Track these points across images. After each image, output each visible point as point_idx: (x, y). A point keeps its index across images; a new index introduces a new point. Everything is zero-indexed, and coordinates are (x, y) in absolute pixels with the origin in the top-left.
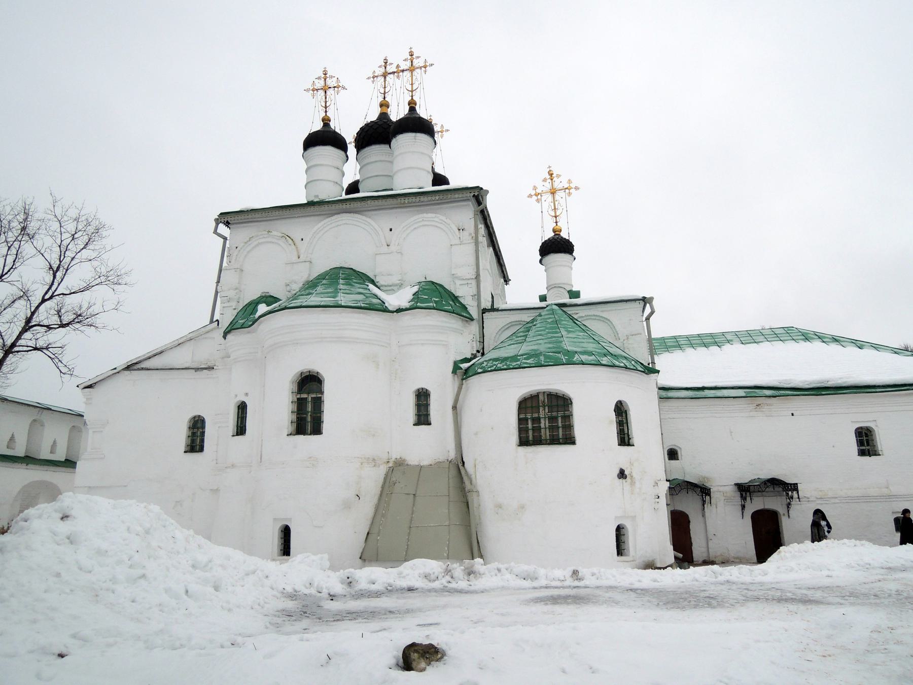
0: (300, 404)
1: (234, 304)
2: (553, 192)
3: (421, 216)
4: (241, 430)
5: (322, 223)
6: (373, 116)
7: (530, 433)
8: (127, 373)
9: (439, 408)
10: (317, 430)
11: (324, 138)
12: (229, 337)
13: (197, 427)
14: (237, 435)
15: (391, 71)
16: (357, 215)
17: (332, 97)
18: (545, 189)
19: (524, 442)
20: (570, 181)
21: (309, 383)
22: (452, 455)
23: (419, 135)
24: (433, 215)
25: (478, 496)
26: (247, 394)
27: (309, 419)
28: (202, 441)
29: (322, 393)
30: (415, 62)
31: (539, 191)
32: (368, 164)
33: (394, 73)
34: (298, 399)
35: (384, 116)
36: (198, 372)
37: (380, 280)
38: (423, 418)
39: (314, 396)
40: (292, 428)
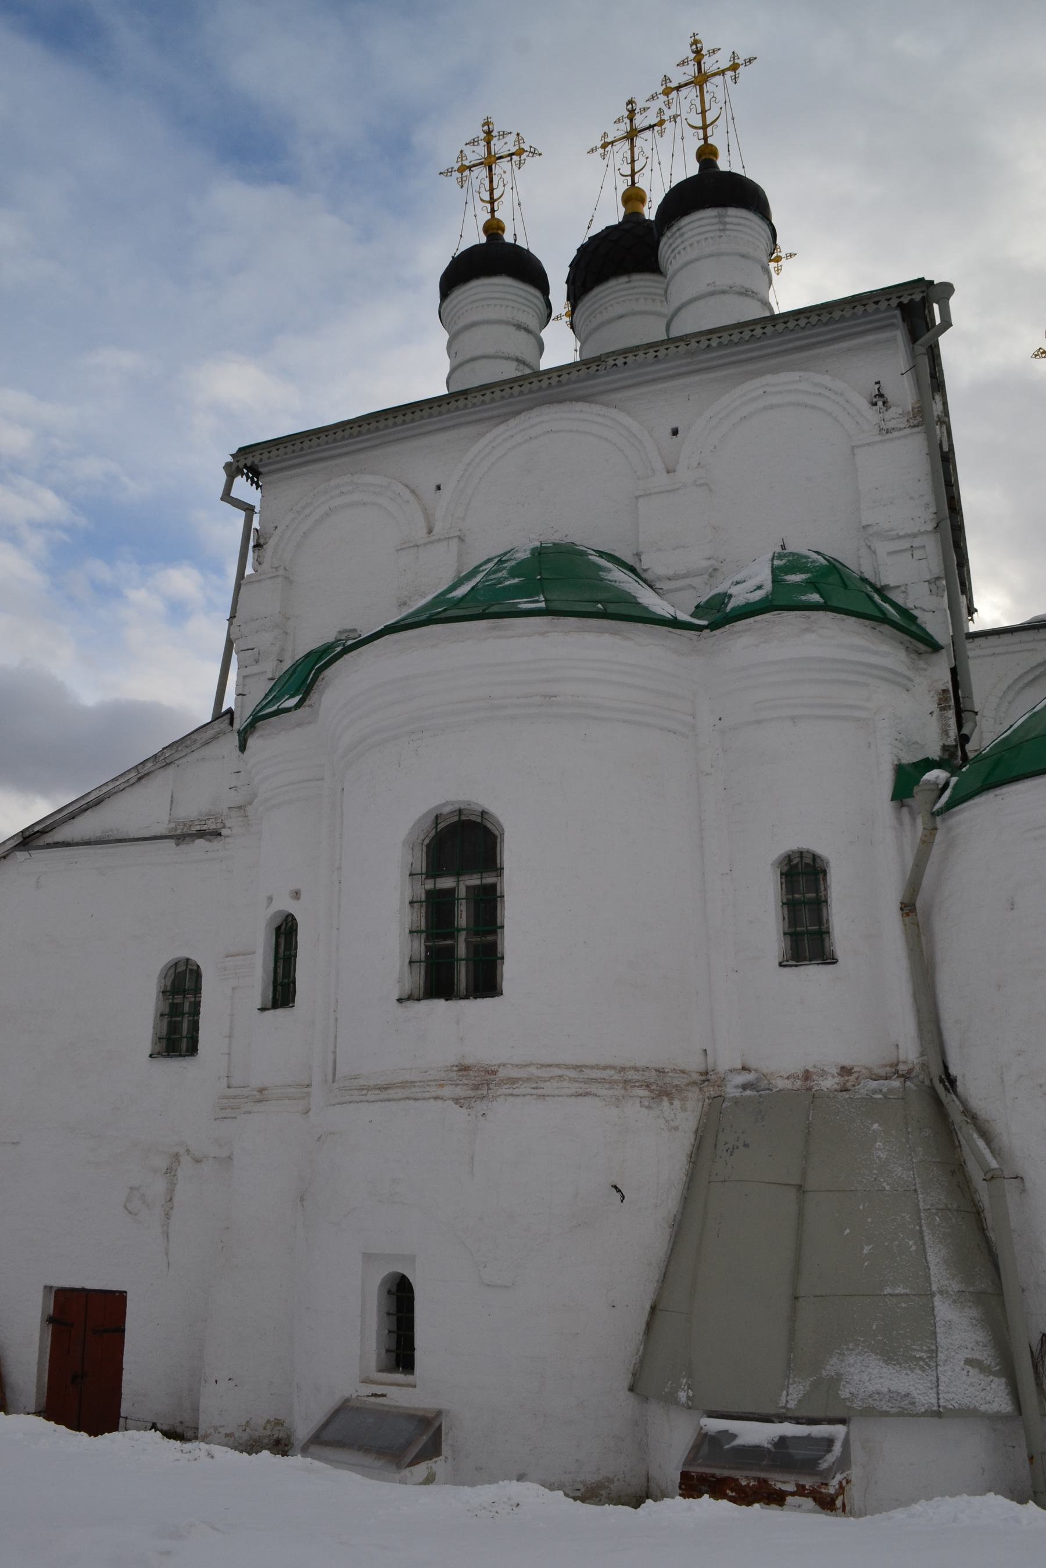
0: (437, 912)
3: (757, 382)
4: (282, 993)
5: (489, 437)
6: (613, 215)
8: (21, 855)
10: (486, 984)
13: (182, 987)
15: (646, 124)
16: (579, 406)
21: (462, 847)
22: (910, 1052)
23: (732, 211)
24: (794, 375)
26: (296, 895)
27: (462, 950)
28: (195, 1027)
29: (499, 871)
32: (603, 324)
33: (651, 127)
34: (428, 893)
35: (633, 218)
37: (653, 564)
38: (807, 937)
39: (474, 881)
40: (415, 979)
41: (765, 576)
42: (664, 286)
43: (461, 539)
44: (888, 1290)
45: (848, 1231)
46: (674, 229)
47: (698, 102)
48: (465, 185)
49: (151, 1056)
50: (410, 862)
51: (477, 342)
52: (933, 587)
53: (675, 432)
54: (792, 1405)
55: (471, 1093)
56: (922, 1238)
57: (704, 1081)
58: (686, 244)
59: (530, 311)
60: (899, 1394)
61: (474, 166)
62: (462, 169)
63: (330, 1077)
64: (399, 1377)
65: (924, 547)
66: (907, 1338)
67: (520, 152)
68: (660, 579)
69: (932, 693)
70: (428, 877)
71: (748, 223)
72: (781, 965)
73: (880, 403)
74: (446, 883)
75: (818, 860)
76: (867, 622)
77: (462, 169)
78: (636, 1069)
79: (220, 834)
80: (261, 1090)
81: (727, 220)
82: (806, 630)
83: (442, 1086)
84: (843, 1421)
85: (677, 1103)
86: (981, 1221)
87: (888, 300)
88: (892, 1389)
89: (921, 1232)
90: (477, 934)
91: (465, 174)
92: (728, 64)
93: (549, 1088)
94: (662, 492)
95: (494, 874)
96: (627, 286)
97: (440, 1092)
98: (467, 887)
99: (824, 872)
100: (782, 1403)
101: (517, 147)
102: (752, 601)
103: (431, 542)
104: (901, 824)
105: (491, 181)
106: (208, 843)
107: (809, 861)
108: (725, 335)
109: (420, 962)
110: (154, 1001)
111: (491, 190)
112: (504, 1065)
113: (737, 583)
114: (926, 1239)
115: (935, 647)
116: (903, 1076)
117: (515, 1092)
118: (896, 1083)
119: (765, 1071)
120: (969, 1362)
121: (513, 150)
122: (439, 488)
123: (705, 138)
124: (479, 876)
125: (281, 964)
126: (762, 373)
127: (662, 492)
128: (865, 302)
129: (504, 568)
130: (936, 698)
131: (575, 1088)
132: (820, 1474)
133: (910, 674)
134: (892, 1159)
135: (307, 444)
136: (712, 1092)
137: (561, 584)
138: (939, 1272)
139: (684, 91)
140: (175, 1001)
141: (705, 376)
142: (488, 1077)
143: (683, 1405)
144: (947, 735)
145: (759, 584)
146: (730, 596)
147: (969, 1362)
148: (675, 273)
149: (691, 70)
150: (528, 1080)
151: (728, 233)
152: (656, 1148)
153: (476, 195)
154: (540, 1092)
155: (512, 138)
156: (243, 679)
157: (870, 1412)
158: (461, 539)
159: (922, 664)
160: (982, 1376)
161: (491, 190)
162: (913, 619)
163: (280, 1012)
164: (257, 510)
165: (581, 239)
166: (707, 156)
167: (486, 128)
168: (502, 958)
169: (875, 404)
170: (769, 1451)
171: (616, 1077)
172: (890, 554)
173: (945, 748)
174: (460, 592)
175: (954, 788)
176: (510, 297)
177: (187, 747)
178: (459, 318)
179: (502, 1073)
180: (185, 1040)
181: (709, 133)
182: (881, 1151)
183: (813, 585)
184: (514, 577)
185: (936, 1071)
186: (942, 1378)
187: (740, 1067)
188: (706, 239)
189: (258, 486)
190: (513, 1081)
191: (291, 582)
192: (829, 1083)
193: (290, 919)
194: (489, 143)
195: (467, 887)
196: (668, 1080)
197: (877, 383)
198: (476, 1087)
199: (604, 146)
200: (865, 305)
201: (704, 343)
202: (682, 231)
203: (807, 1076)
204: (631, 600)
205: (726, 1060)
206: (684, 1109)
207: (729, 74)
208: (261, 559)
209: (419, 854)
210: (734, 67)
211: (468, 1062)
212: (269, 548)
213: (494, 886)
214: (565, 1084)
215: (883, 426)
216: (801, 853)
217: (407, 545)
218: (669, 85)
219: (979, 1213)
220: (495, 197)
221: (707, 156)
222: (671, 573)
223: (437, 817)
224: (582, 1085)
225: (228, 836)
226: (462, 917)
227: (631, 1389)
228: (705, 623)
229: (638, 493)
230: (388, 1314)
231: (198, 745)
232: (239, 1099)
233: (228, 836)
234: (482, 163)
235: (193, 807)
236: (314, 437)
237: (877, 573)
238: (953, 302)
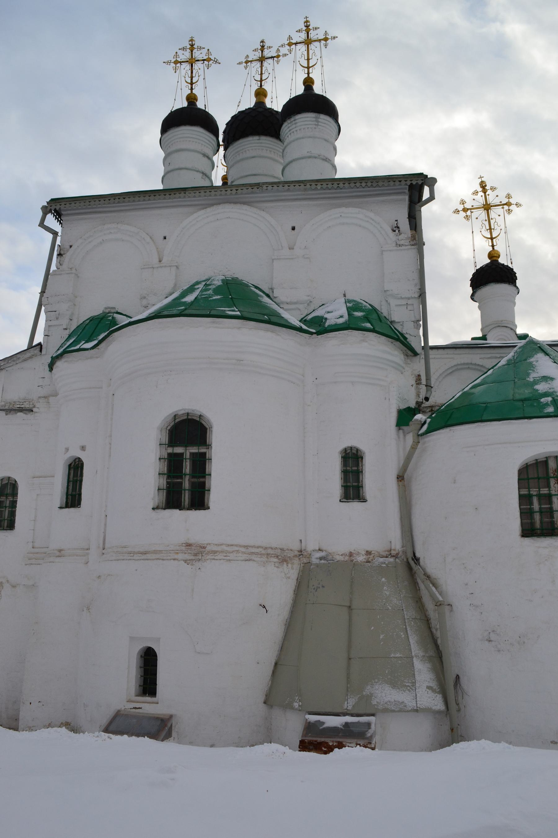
0: (173, 465)
2: (487, 207)
4: (73, 499)
5: (196, 215)
6: (249, 102)
7: (537, 517)
9: (378, 477)
10: (199, 501)
11: (188, 116)
12: (59, 364)
15: (270, 55)
16: (245, 207)
17: (201, 72)
18: (476, 205)
19: (528, 531)
20: (509, 196)
22: (397, 545)
23: (322, 116)
24: (357, 210)
25: (451, 611)
27: (186, 484)
28: (13, 514)
29: (209, 446)
30: (312, 35)
31: (468, 206)
32: (242, 160)
33: (272, 57)
35: (260, 104)
36: (10, 416)
38: (352, 488)
39: (194, 450)
41: (343, 311)
42: (282, 148)
43: (177, 267)
44: (392, 655)
45: (373, 628)
46: (292, 119)
47: (306, 53)
48: (178, 72)
51: (181, 160)
52: (416, 324)
53: (293, 228)
54: (350, 708)
55: (193, 558)
56: (407, 631)
57: (300, 555)
58: (297, 129)
59: (209, 147)
60: (399, 702)
61: (183, 62)
62: (176, 62)
63: (101, 546)
64: (148, 699)
65: (413, 304)
66: (402, 678)
67: (209, 60)
68: (283, 303)
69: (413, 376)
71: (329, 123)
72: (340, 501)
73: (397, 231)
74: (179, 450)
75: (359, 452)
76: (390, 340)
77: (176, 62)
78: (272, 548)
79: (32, 411)
80: (60, 551)
81: (320, 120)
82: (364, 341)
83: (177, 553)
84: (373, 715)
85: (290, 565)
86: (429, 624)
87: (406, 181)
88: (396, 700)
89: (406, 629)
90: (193, 477)
91: (177, 65)
92: (323, 37)
93: (232, 556)
94: (287, 259)
95: (205, 447)
96: (258, 141)
97: (176, 556)
98: (190, 453)
99: (362, 458)
100: (345, 707)
101: (207, 57)
102: (338, 323)
103: (161, 267)
104: (399, 438)
105: (192, 72)
107: (354, 452)
108: (324, 184)
109: (164, 489)
111: (192, 78)
112: (210, 544)
113: (328, 312)
114: (409, 632)
115: (415, 354)
116: (394, 556)
117: (216, 558)
118: (392, 560)
119: (330, 552)
120: (428, 687)
121: (205, 58)
122: (165, 238)
123: (308, 73)
124: (197, 448)
125: (71, 484)
126: (340, 206)
127: (287, 259)
128: (394, 180)
129: (210, 289)
130: (415, 378)
131: (245, 557)
132: (367, 738)
133: (404, 365)
134: (391, 595)
135: (92, 203)
136: (305, 561)
137: (235, 300)
138: (415, 649)
139: (299, 46)
141: (311, 202)
142: (201, 550)
143: (296, 709)
144: (419, 396)
145: (341, 315)
146: (326, 319)
147: (428, 687)
148: (290, 143)
149: (303, 36)
150: (222, 552)
151: (319, 127)
152: (278, 587)
153: (183, 79)
154: (228, 558)
155: (205, 51)
156: (48, 327)
157: (386, 710)
158: (177, 267)
159: (409, 361)
160: (433, 694)
161: (192, 78)
162: (406, 338)
163: (72, 510)
164: (60, 234)
165: (234, 112)
166: (308, 83)
167: (191, 42)
168: (209, 490)
169: (395, 231)
170: (341, 729)
171: (263, 552)
172: (397, 305)
173: (417, 403)
174: (190, 298)
175: (429, 424)
176: (194, 136)
177: (14, 361)
178: (172, 145)
179: (209, 548)
181: (310, 71)
182: (386, 591)
183: (366, 319)
184: (217, 295)
185: (410, 555)
186: (418, 695)
187: (318, 549)
188: (308, 128)
189: (60, 223)
190: (215, 552)
191: (78, 277)
192: (361, 558)
193: (77, 460)
194: (192, 51)
195: (190, 453)
196: (285, 554)
197: (396, 221)
198: (196, 555)
199: (247, 62)
200: (394, 181)
201: (314, 186)
202: (296, 121)
203: (351, 554)
204: (279, 316)
205: (311, 546)
206: (292, 568)
207: (323, 42)
208: (61, 262)
210: (326, 39)
211: (191, 541)
212: (67, 257)
213: (205, 454)
214: (240, 554)
215: (398, 243)
216: (351, 448)
217: (147, 267)
218: (291, 41)
219: (428, 620)
220: (194, 82)
221: (308, 83)
222: (288, 300)
223: (175, 416)
224: (247, 555)
226: (187, 468)
227: (265, 703)
228: (314, 331)
229: (273, 258)
230: (141, 667)
231: (20, 361)
232: (38, 555)
234: (187, 61)
236: (97, 200)
237: (389, 314)
238: (436, 187)
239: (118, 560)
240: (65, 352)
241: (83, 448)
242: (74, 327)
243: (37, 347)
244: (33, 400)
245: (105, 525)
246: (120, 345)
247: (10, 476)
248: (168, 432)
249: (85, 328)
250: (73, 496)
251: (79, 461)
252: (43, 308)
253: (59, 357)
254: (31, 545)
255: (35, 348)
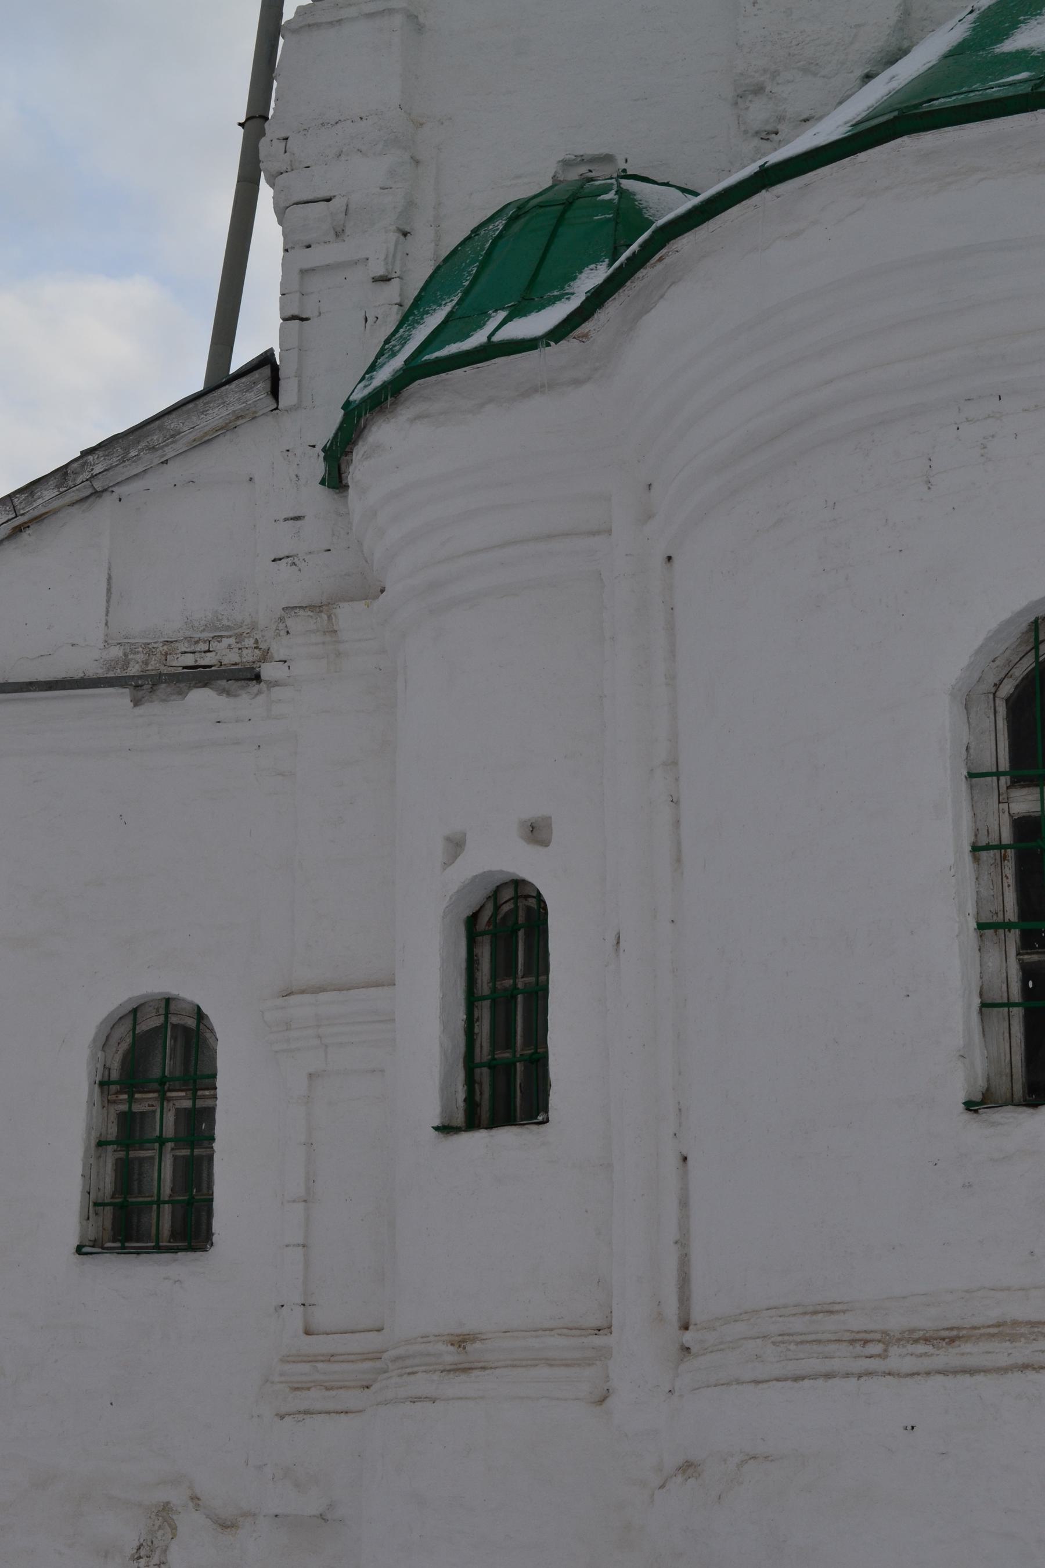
1: (375, 246)
4: (503, 1078)
12: (359, 469)
13: (158, 1081)
14: (473, 1121)
26: (536, 832)
34: (1024, 827)
36: (153, 709)
49: (79, 1250)
50: (965, 742)
63: (672, 1310)
70: (1018, 781)
79: (258, 678)
80: (461, 1342)
106: (223, 699)
110: (84, 1106)
140: (136, 1108)
156: (298, 279)
177: (153, 449)
180: (167, 1209)
193: (507, 894)
209: (988, 723)
225: (276, 684)
231: (181, 445)
233: (276, 684)
235: (168, 609)
239: (797, 1378)
240: (417, 370)
241: (536, 832)
242: (420, 273)
243: (256, 375)
244: (254, 627)
245: (684, 1203)
246: (688, 313)
247: (173, 991)
248: (1002, 710)
249: (489, 253)
250: (502, 1071)
251: (516, 898)
252: (266, 194)
253: (382, 400)
254: (295, 1319)
255: (238, 388)
